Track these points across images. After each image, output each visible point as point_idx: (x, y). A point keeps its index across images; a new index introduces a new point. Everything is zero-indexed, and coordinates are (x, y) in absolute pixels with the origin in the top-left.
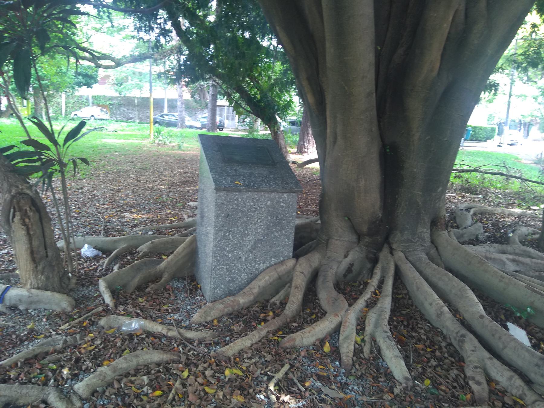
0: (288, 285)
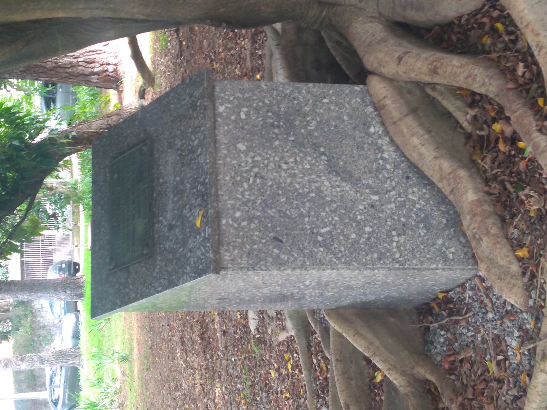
0: (429, 91)
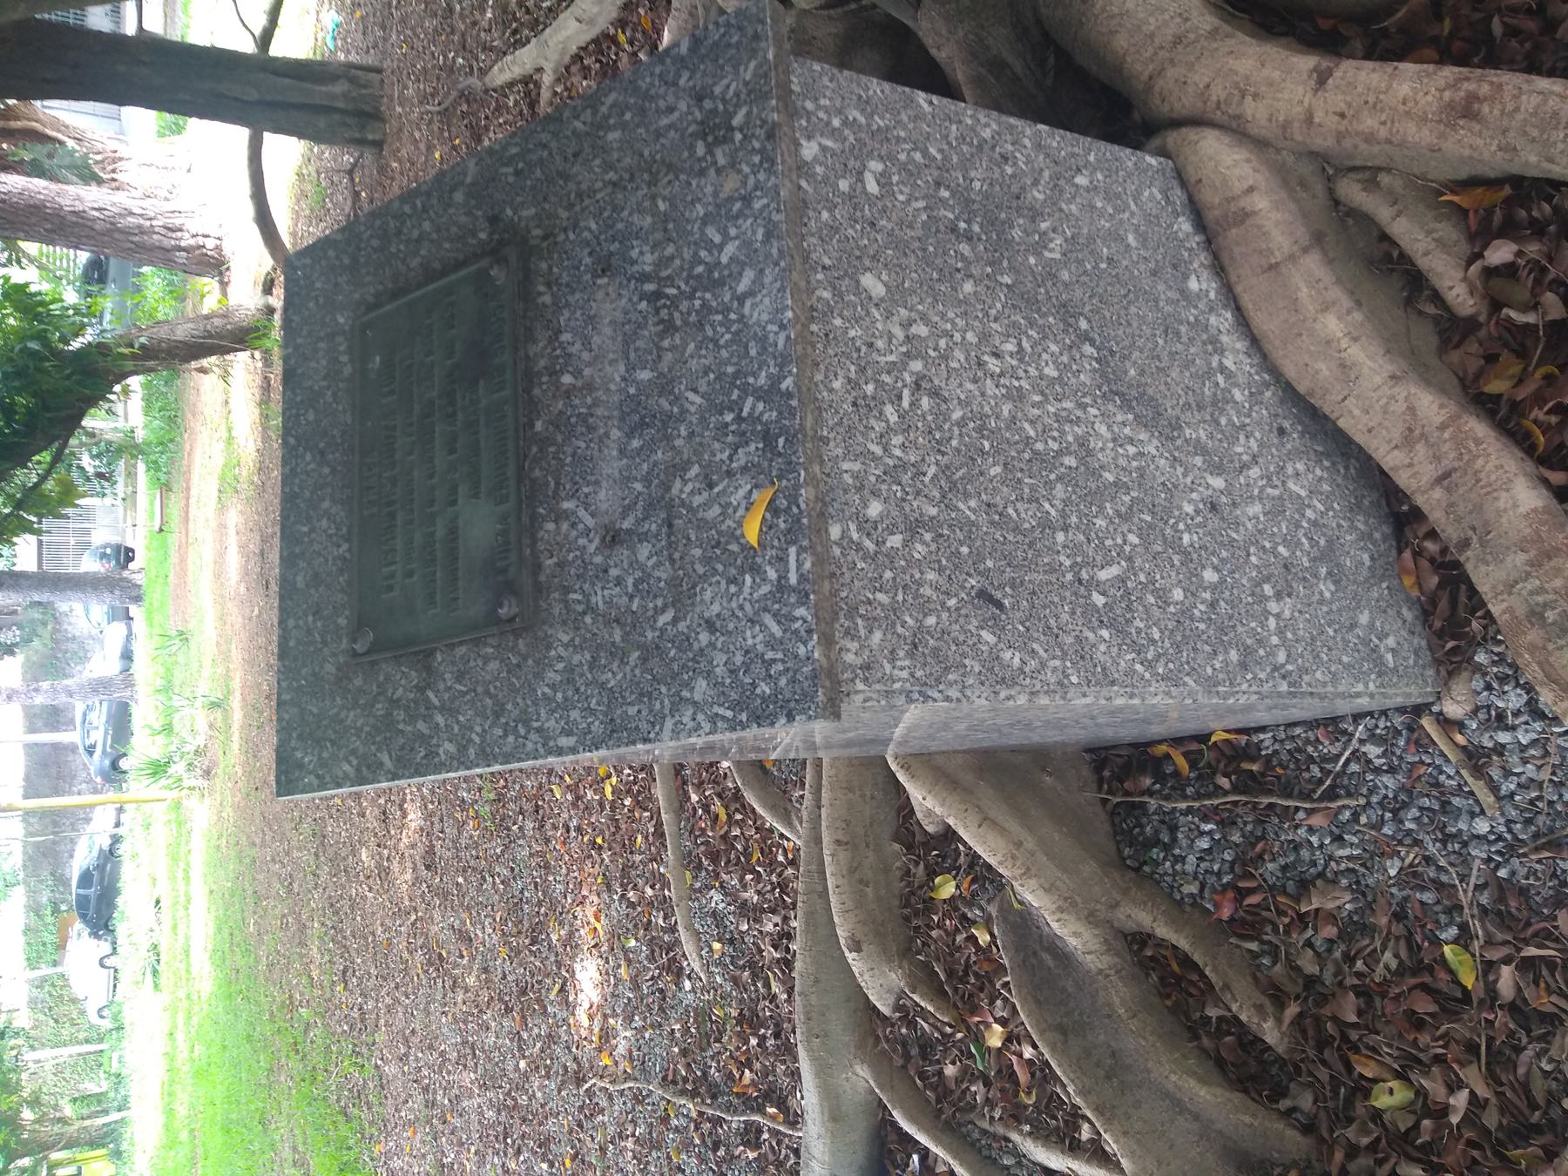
0: (1352, 192)
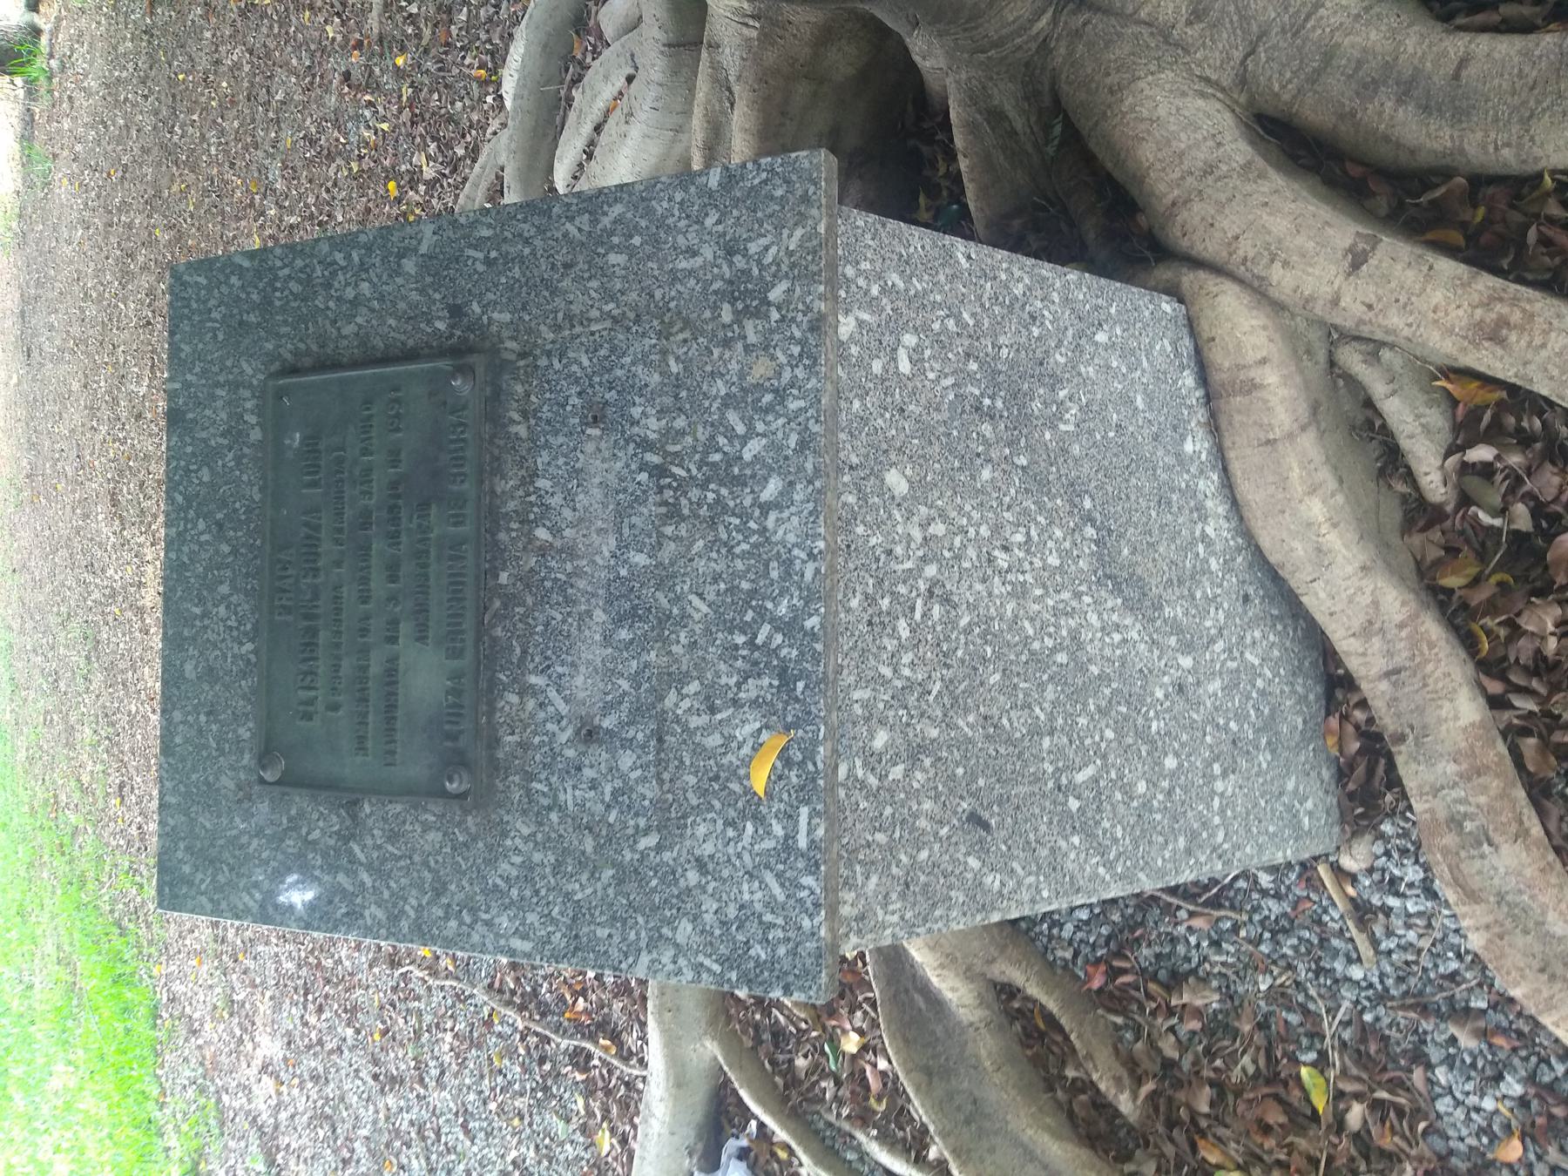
0: (1352, 359)
